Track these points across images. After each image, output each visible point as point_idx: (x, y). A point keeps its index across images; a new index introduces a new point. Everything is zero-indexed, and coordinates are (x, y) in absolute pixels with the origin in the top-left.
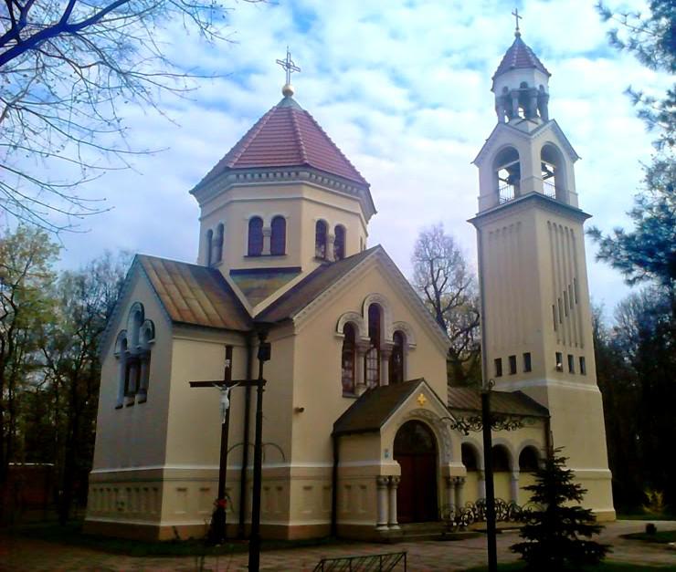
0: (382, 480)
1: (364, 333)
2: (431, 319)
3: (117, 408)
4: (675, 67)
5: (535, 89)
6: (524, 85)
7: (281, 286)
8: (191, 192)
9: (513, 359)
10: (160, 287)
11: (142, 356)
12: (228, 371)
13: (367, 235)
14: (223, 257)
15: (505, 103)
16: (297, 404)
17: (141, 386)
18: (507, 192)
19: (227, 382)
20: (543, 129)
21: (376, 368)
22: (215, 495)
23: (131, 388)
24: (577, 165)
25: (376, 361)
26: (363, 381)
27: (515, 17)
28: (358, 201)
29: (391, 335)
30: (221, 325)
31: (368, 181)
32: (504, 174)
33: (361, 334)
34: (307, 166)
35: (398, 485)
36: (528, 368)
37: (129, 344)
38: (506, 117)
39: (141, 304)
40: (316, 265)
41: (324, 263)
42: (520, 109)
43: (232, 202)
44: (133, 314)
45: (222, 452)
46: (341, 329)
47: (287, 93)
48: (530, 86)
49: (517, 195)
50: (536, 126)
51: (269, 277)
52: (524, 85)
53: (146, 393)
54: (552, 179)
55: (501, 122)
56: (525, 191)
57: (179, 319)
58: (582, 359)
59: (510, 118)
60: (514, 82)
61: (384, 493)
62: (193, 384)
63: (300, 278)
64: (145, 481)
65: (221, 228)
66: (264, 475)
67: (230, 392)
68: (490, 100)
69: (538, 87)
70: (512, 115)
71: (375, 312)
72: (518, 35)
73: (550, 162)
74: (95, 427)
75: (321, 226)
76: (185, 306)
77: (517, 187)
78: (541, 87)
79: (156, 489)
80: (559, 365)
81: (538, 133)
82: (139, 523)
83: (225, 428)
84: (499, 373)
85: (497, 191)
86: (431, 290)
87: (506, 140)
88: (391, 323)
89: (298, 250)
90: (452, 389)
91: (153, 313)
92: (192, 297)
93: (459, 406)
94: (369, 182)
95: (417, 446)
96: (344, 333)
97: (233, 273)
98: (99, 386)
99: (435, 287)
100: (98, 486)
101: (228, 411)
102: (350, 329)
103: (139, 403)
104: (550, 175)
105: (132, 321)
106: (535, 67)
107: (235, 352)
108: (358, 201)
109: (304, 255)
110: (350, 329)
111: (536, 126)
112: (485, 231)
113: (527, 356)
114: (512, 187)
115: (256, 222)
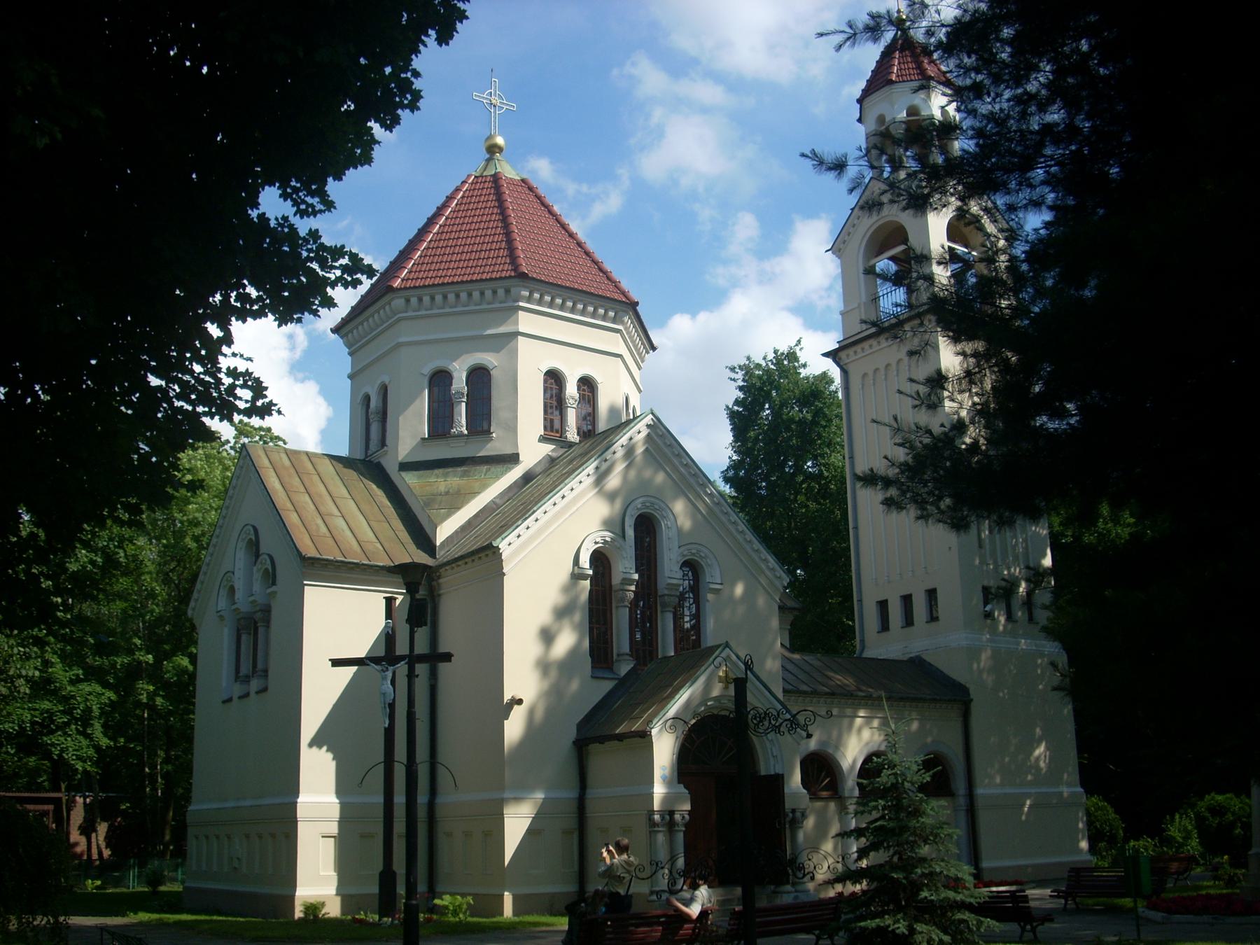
3: (224, 702)
7: (484, 487)
11: (259, 616)
14: (388, 442)
17: (260, 666)
23: (245, 669)
29: (676, 568)
31: (635, 296)
34: (523, 276)
37: (239, 595)
39: (254, 527)
43: (399, 345)
46: (585, 561)
51: (465, 474)
53: (266, 676)
63: (515, 474)
65: (384, 390)
67: (394, 673)
74: (356, 168)
75: (554, 379)
76: (323, 529)
84: (885, 627)
88: (676, 544)
89: (512, 428)
93: (805, 688)
97: (405, 467)
98: (459, 508)
103: (257, 693)
113: (932, 594)
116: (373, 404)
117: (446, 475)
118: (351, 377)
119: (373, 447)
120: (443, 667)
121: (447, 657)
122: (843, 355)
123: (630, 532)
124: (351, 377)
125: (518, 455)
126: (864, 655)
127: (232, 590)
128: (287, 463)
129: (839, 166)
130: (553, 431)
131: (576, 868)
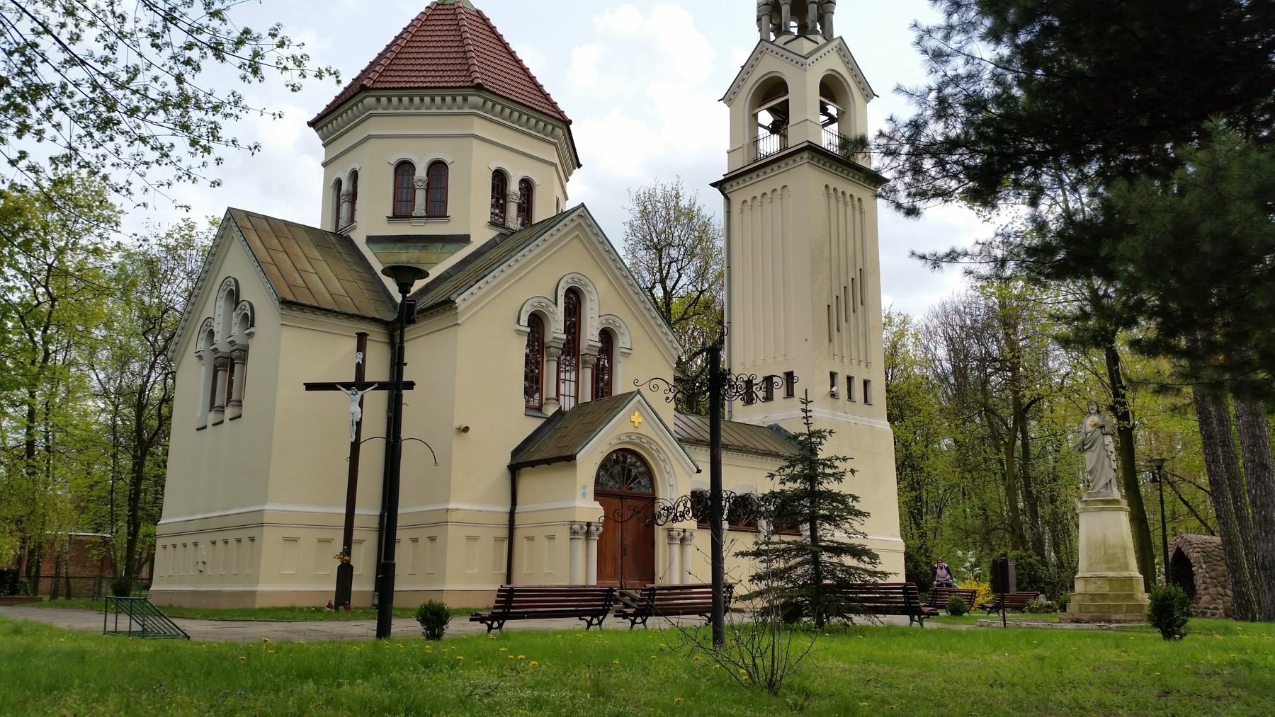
0: (576, 527)
1: (556, 329)
8: (311, 124)
10: (262, 253)
12: (360, 369)
13: (566, 199)
14: (356, 219)
16: (460, 422)
17: (234, 397)
18: (770, 145)
19: (360, 384)
21: (573, 394)
22: (339, 546)
24: (873, 105)
25: (573, 384)
26: (554, 395)
28: (555, 144)
29: (597, 333)
30: (353, 311)
31: (569, 116)
32: (765, 118)
33: (553, 329)
34: (479, 87)
35: (601, 536)
37: (217, 337)
38: (772, 35)
39: (236, 282)
40: (491, 234)
41: (504, 231)
42: (793, 24)
44: (223, 294)
54: (835, 127)
56: (796, 137)
57: (290, 298)
58: (866, 383)
59: (777, 36)
62: (310, 387)
65: (354, 175)
70: (780, 30)
71: (574, 300)
73: (833, 100)
75: (500, 178)
76: (300, 282)
77: (784, 137)
81: (817, 55)
82: (227, 588)
83: (355, 447)
85: (756, 142)
86: (658, 292)
87: (771, 65)
90: (682, 417)
91: (255, 292)
92: (311, 269)
94: (569, 117)
95: (626, 478)
97: (371, 240)
99: (664, 288)
100: (169, 542)
101: (359, 424)
102: (537, 321)
104: (832, 120)
105: (221, 303)
107: (370, 347)
108: (555, 144)
109: (471, 214)
110: (537, 321)
112: (737, 199)
114: (776, 137)
115: (404, 168)
118: (325, 165)
119: (342, 223)
121: (410, 385)
122: (727, 185)
123: (561, 300)
124: (325, 165)
125: (469, 236)
126: (708, 437)
127: (211, 333)
128: (268, 228)
130: (498, 220)
131: (505, 570)
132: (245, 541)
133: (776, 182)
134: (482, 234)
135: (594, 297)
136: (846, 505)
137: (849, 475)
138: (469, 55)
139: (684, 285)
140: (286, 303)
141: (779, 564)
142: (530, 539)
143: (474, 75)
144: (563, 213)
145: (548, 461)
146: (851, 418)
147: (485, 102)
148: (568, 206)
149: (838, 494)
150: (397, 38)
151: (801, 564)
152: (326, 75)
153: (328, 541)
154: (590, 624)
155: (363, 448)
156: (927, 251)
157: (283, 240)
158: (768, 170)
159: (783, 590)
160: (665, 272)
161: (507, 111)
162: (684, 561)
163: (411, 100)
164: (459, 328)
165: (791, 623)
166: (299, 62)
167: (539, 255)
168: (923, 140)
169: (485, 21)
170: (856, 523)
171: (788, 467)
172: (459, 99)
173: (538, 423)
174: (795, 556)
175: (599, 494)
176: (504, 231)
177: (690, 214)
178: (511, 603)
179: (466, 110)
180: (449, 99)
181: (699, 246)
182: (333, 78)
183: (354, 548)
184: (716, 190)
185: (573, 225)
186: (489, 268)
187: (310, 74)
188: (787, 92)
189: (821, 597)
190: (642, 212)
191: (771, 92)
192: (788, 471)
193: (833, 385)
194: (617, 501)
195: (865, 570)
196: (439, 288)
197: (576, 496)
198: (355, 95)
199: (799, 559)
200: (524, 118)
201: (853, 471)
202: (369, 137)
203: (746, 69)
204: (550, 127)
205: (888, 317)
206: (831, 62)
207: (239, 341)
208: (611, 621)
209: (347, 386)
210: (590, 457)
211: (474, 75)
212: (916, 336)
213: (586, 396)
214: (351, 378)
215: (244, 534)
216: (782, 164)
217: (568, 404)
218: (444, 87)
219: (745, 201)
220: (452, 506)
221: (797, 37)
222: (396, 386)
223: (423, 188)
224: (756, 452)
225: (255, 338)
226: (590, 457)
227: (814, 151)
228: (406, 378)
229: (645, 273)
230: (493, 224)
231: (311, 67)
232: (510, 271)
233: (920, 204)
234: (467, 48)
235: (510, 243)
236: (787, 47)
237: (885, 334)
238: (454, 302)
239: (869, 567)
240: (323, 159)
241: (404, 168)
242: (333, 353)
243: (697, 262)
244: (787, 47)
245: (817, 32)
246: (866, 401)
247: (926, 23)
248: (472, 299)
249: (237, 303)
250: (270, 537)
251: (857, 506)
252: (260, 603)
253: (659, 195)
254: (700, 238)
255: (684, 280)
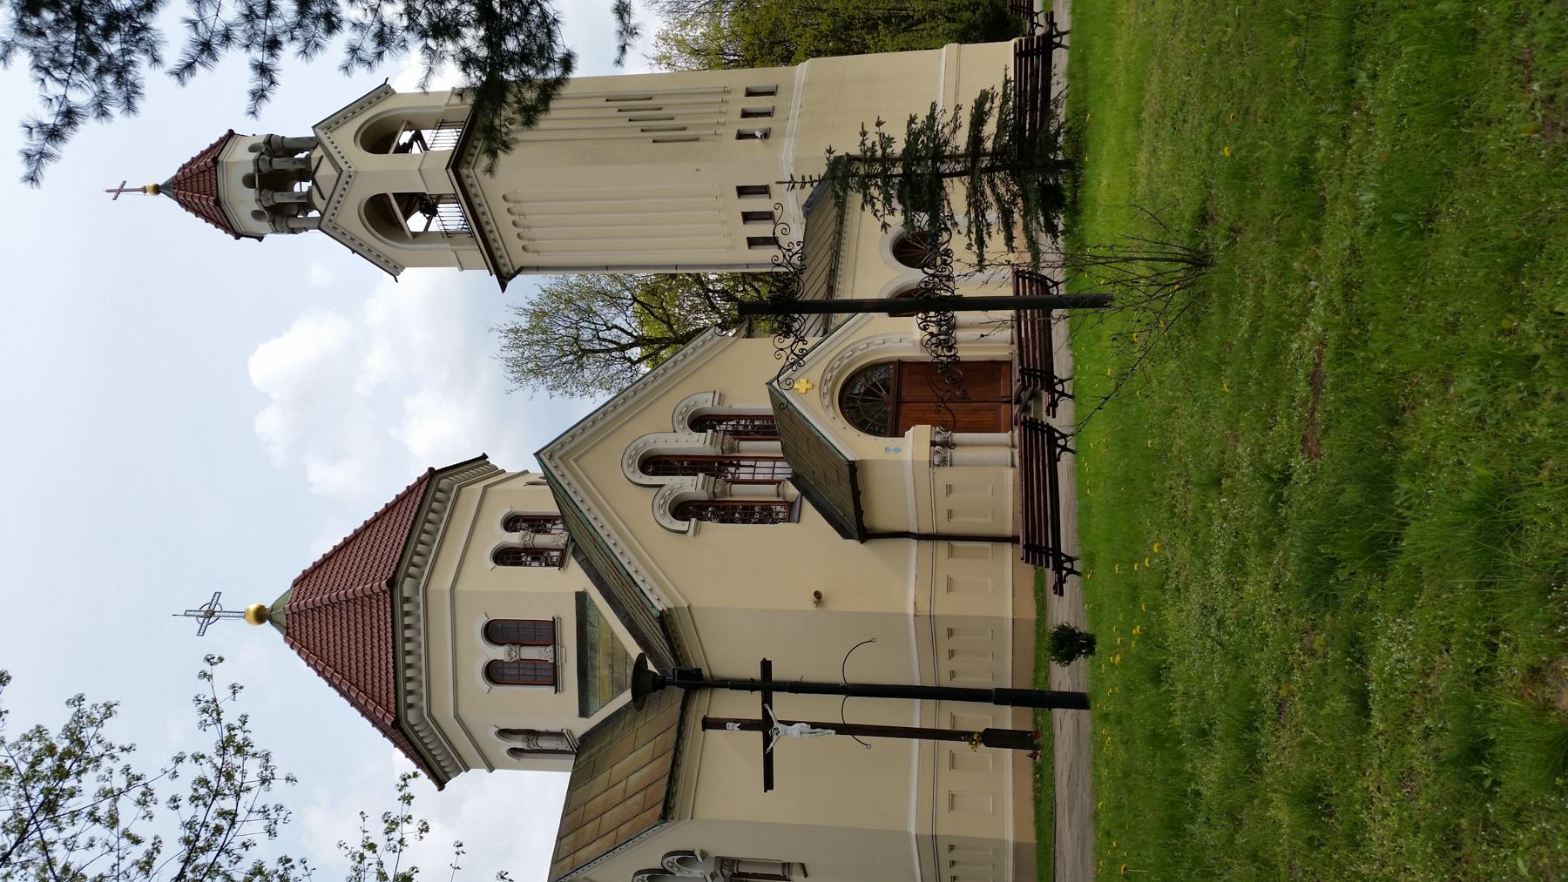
0: (937, 459)
1: (690, 486)
2: (679, 356)
4: (396, 879)
5: (256, 161)
6: (249, 181)
8: (441, 786)
9: (748, 217)
12: (746, 725)
15: (284, 215)
16: (808, 602)
17: (779, 872)
18: (450, 216)
19: (765, 725)
20: (331, 148)
21: (771, 464)
27: (117, 187)
28: (460, 489)
30: (673, 733)
31: (423, 471)
32: (416, 222)
33: (692, 490)
34: (392, 583)
36: (763, 190)
38: (311, 215)
40: (573, 566)
42: (297, 188)
45: (797, 692)
47: (261, 615)
48: (251, 169)
49: (454, 199)
50: (325, 161)
51: (593, 647)
52: (249, 181)
54: (427, 135)
55: (319, 225)
56: (442, 183)
57: (659, 809)
58: (750, 93)
59: (313, 207)
60: (244, 201)
61: (958, 454)
62: (769, 785)
64: (937, 866)
65: (504, 733)
66: (1025, 684)
68: (277, 242)
69: (254, 155)
70: (306, 204)
71: (655, 464)
72: (157, 190)
73: (393, 136)
75: (505, 556)
76: (639, 797)
77: (440, 198)
78: (252, 149)
79: (952, 847)
80: (758, 134)
85: (447, 234)
86: (635, 353)
87: (351, 214)
92: (622, 785)
95: (876, 398)
96: (688, 519)
97: (584, 712)
99: (631, 346)
101: (814, 725)
102: (683, 509)
104: (417, 137)
106: (215, 161)
107: (717, 713)
109: (549, 591)
110: (683, 509)
111: (325, 161)
112: (520, 258)
113: (743, 191)
114: (441, 208)
115: (493, 673)
116: (519, 745)
117: (594, 668)
118: (491, 769)
119: (563, 746)
120: (777, 674)
121: (766, 666)
122: (504, 270)
123: (657, 480)
124: (491, 769)
125: (577, 594)
128: (571, 837)
129: (70, 116)
131: (988, 545)
132: (954, 856)
133: (499, 208)
134: (575, 578)
135: (651, 438)
136: (921, 131)
137: (883, 129)
138: (351, 596)
139: (625, 321)
140: (666, 815)
141: (992, 215)
142: (950, 514)
143: (376, 590)
144: (546, 477)
145: (856, 495)
146: (794, 113)
147: (410, 576)
148: (536, 469)
149: (907, 142)
150: (331, 684)
151: (993, 188)
152: (407, 791)
153: (952, 756)
154: (1064, 448)
155: (851, 720)
156: (615, 43)
157: (586, 819)
158: (483, 219)
159: (1026, 213)
160: (612, 346)
161: (420, 548)
162: (985, 338)
163: (409, 666)
164: (694, 604)
165: (1064, 198)
166: (392, 825)
167: (605, 513)
168: (483, 53)
169: (306, 575)
170: (943, 119)
171: (873, 205)
172: (407, 607)
173: (807, 506)
174: (983, 194)
175: (897, 432)
176: (570, 549)
177: (538, 315)
178: (1039, 543)
179: (420, 598)
180: (407, 620)
181: (579, 304)
182: (411, 782)
183: (961, 727)
184: (510, 284)
185: (562, 466)
186: (618, 568)
187: (406, 810)
188: (385, 195)
189: (1032, 158)
190: (536, 375)
191: (384, 215)
192: (879, 206)
193: (753, 136)
194: (904, 409)
195: (1001, 108)
196: (644, 630)
197: (899, 460)
198: (405, 734)
199: (988, 191)
200: (428, 526)
201: (879, 124)
202: (457, 717)
203: (356, 247)
204: (439, 495)
205: (659, 60)
206: (345, 140)
207: (710, 868)
208: (1062, 419)
209: (767, 740)
210: (852, 443)
211: (376, 590)
212: (684, 25)
213: (774, 447)
214: (758, 736)
215: (945, 857)
216: (476, 201)
217: (783, 470)
218: (393, 627)
219: (524, 248)
220: (911, 611)
221: (314, 182)
222: (766, 684)
223: (519, 649)
224: (839, 234)
225: (706, 848)
226: (852, 443)
227: (458, 160)
228: (756, 674)
229: (613, 370)
230: (561, 563)
231: (398, 809)
232: (621, 544)
233: (559, 53)
234: (342, 598)
235: (586, 544)
236: (327, 196)
237: (681, 63)
238: (662, 612)
239: (998, 102)
240: (484, 771)
241: (493, 673)
242: (726, 761)
243: (598, 306)
244: (327, 196)
245: (308, 157)
246: (772, 93)
247: (343, 56)
248: (657, 590)
249: (665, 871)
250: (949, 827)
251: (922, 118)
252: (1030, 837)
253: (514, 354)
254: (569, 301)
255: (620, 321)
